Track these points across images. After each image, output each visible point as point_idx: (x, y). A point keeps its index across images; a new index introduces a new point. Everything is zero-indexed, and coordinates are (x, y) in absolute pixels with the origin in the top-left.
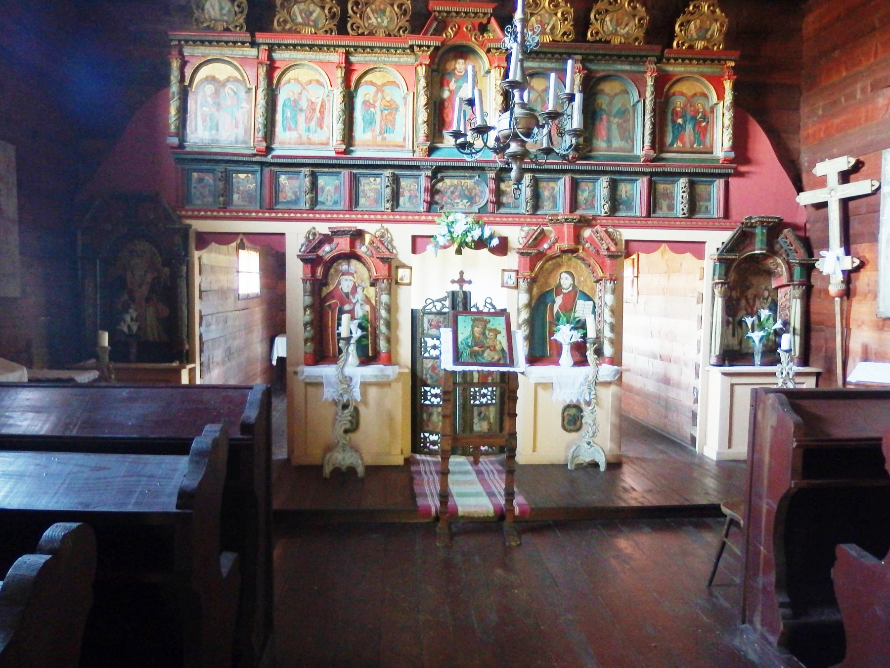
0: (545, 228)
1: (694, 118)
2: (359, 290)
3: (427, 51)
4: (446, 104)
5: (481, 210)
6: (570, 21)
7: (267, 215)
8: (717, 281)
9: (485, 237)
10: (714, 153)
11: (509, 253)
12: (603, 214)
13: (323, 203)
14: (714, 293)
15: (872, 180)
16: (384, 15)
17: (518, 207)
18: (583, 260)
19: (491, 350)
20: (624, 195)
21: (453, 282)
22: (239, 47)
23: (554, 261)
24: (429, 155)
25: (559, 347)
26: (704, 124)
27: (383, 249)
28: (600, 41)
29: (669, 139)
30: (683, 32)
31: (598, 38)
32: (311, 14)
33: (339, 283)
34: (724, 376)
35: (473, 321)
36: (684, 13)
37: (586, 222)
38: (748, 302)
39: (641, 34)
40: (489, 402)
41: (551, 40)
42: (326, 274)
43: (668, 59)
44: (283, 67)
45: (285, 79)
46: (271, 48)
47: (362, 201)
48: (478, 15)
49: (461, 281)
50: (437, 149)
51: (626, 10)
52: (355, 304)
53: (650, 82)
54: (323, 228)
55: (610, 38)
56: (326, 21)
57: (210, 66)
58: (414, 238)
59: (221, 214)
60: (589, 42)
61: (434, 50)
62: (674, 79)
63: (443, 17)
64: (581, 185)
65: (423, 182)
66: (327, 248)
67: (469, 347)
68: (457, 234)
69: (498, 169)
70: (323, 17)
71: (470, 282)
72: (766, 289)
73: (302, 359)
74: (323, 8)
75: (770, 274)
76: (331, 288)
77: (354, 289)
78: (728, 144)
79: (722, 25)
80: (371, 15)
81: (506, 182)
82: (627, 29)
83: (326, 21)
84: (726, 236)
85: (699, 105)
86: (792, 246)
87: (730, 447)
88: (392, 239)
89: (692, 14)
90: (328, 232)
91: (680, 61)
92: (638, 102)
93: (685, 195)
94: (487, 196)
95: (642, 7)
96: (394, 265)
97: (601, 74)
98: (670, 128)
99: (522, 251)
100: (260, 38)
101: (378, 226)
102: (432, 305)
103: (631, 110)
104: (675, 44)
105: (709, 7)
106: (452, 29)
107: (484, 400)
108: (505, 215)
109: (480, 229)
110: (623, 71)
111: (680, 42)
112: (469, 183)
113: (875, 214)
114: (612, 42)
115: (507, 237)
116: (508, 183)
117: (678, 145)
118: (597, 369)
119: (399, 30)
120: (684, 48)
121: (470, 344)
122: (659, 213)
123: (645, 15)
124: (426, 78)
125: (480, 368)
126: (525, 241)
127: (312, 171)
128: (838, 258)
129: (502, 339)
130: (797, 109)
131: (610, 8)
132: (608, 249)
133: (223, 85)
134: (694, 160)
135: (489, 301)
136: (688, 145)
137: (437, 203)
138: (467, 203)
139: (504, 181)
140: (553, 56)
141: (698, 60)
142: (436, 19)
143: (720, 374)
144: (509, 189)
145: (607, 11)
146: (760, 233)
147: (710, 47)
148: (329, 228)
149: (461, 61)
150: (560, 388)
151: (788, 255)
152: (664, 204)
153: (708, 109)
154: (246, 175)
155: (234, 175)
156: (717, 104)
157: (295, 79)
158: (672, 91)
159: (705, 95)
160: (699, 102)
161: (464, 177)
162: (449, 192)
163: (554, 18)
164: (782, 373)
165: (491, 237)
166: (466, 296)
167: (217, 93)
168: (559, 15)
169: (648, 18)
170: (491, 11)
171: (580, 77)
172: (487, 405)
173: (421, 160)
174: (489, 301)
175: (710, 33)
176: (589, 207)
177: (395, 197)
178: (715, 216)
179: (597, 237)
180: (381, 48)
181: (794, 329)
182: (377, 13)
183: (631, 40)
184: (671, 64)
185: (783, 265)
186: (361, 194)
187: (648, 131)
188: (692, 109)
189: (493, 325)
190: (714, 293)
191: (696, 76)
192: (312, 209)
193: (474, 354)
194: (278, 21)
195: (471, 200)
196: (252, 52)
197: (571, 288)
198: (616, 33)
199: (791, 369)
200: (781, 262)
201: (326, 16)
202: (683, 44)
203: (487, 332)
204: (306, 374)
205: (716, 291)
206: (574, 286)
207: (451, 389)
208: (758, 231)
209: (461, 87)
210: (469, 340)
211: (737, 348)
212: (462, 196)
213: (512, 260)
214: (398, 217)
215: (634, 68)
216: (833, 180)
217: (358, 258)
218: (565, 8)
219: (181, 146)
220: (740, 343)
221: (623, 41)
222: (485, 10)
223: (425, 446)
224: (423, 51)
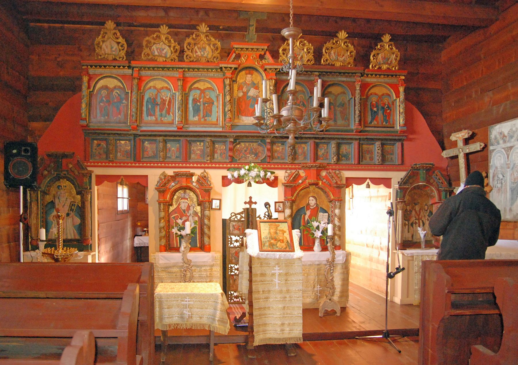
2: (191, 208)
3: (230, 70)
21: (245, 203)
26: (388, 111)
30: (375, 60)
32: (163, 50)
43: (367, 75)
49: (250, 202)
54: (170, 172)
60: (322, 65)
70: (170, 51)
71: (256, 203)
72: (426, 205)
74: (170, 46)
75: (430, 196)
77: (189, 207)
78: (402, 122)
79: (396, 56)
80: (198, 50)
82: (343, 58)
84: (403, 174)
90: (172, 174)
92: (352, 98)
104: (371, 66)
105: (389, 46)
106: (244, 57)
114: (335, 65)
120: (376, 68)
122: (364, 162)
136: (380, 123)
138: (254, 156)
141: (384, 75)
148: (174, 172)
152: (368, 156)
158: (370, 93)
159: (389, 95)
163: (302, 52)
168: (305, 50)
175: (390, 60)
178: (397, 163)
179: (330, 176)
193: (271, 245)
194: (144, 54)
197: (315, 206)
198: (337, 60)
202: (375, 66)
206: (317, 204)
211: (410, 239)
215: (349, 79)
221: (342, 64)
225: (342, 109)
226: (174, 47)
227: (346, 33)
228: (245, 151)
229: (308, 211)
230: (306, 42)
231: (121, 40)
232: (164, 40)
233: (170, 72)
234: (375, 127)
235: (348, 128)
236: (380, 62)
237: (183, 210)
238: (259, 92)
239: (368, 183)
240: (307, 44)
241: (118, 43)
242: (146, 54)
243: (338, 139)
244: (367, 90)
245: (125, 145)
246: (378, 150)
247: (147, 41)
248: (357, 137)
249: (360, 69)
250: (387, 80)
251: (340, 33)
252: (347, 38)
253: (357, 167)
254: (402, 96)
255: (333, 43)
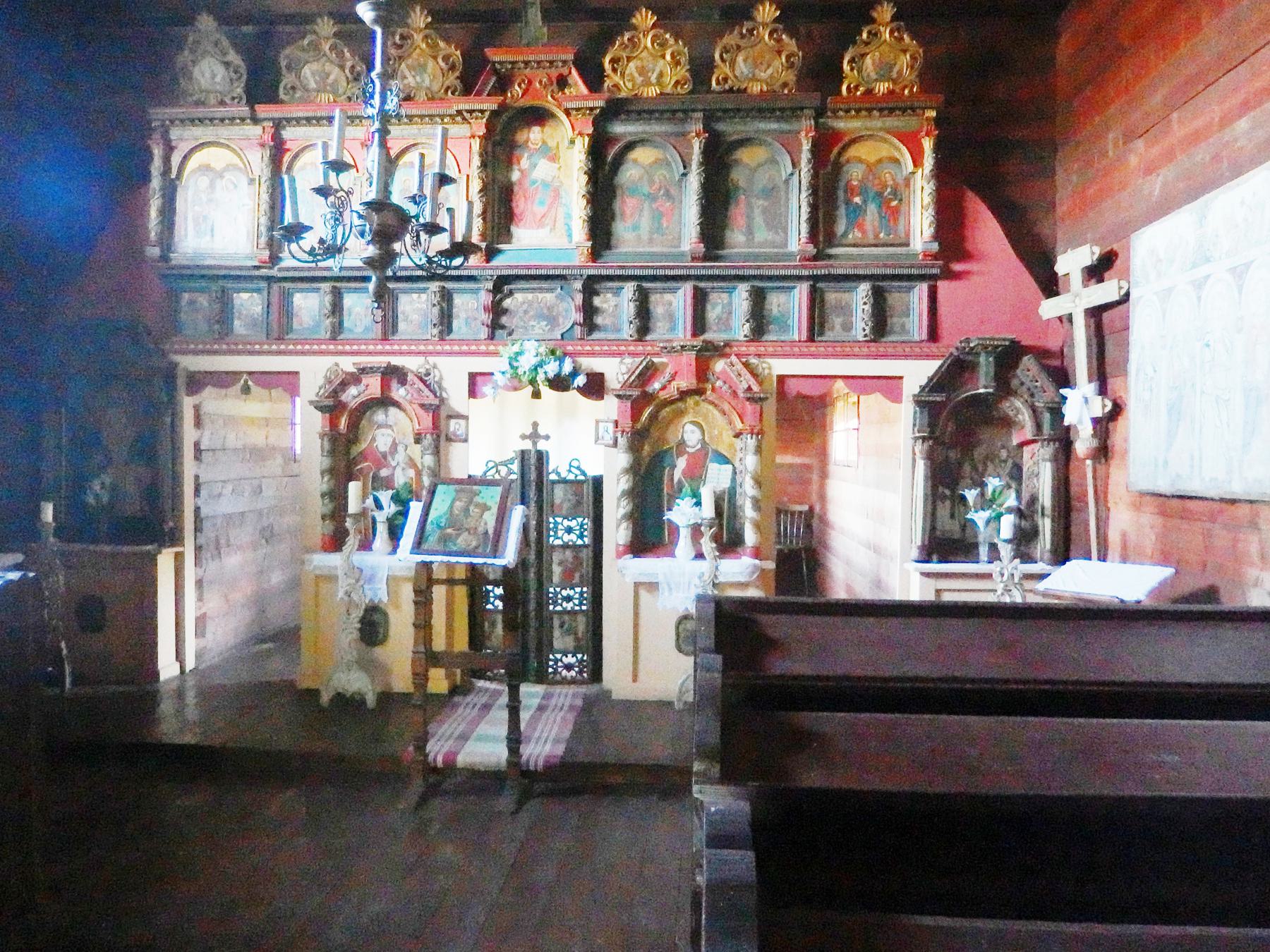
0: (656, 360)
1: (880, 194)
2: (400, 448)
3: (482, 118)
4: (516, 189)
5: (565, 335)
6: (685, 65)
7: (274, 347)
8: (917, 435)
9: (563, 373)
10: (912, 245)
11: (605, 396)
12: (861, 339)
13: (350, 330)
14: (914, 454)
15: (1119, 280)
16: (425, 71)
17: (619, 330)
18: (712, 403)
19: (469, 533)
20: (775, 311)
21: (524, 437)
22: (237, 124)
23: (673, 406)
24: (488, 261)
25: (674, 530)
26: (894, 203)
27: (427, 392)
28: (731, 90)
29: (841, 227)
30: (855, 72)
31: (727, 87)
32: (328, 75)
33: (374, 439)
34: (926, 579)
35: (457, 491)
36: (855, 43)
37: (719, 350)
38: (975, 468)
39: (790, 77)
40: (577, 608)
41: (659, 92)
42: (354, 425)
43: (835, 112)
44: (295, 150)
45: (298, 164)
46: (278, 125)
47: (402, 326)
48: (555, 64)
49: (534, 436)
50: (499, 251)
51: (767, 44)
52: (395, 468)
53: (806, 146)
54: (348, 364)
55: (745, 85)
56: (348, 84)
57: (212, 149)
58: (473, 377)
59: (216, 347)
60: (713, 92)
61: (490, 117)
62: (846, 139)
63: (507, 69)
64: (711, 297)
65: (485, 298)
66: (353, 391)
67: (439, 527)
68: (523, 370)
69: (585, 277)
70: (344, 79)
71: (547, 437)
72: (1003, 447)
73: (320, 543)
74: (342, 67)
75: (1008, 423)
76: (363, 446)
77: (394, 446)
78: (929, 231)
79: (913, 58)
80: (407, 73)
81: (602, 295)
82: (770, 71)
83: (348, 84)
84: (930, 367)
85: (887, 175)
86: (1037, 381)
87: (635, 680)
88: (441, 378)
89: (867, 44)
90: (352, 369)
91: (853, 113)
92: (792, 174)
93: (867, 307)
94: (571, 314)
95: (791, 39)
96: (443, 413)
97: (735, 137)
98: (842, 211)
99: (621, 393)
100: (263, 110)
101: (421, 359)
102: (494, 470)
103: (782, 186)
104: (844, 88)
105: (891, 32)
106: (519, 85)
107: (569, 606)
108: (615, 342)
109: (558, 363)
110: (768, 132)
111: (852, 86)
112: (549, 297)
113: (1125, 332)
114: (749, 91)
115: (602, 374)
116: (605, 296)
117: (855, 235)
118: (715, 564)
119: (446, 91)
120: (858, 93)
121: (443, 525)
122: (829, 335)
123: (796, 49)
124: (481, 155)
125: (446, 559)
126: (626, 377)
127: (334, 287)
128: (1086, 400)
129: (490, 519)
130: (1053, 172)
131: (742, 43)
132: (749, 389)
133: (221, 175)
134: (877, 257)
135: (575, 464)
136: (871, 236)
137: (503, 327)
138: (546, 326)
139: (598, 294)
140: (674, 115)
141: (881, 110)
142: (496, 72)
143: (918, 574)
144: (605, 306)
145: (739, 47)
146: (986, 365)
147: (897, 90)
148: (354, 364)
149: (536, 129)
150: (670, 589)
151: (1032, 395)
152: (837, 321)
153: (900, 180)
154: (250, 294)
155: (235, 295)
156: (913, 173)
157: (312, 163)
158: (843, 159)
159: (896, 161)
160: (886, 171)
161: (541, 290)
162: (521, 310)
163: (662, 62)
164: (1002, 575)
165: (575, 373)
166: (541, 457)
167: (212, 186)
168: (668, 57)
169: (800, 54)
170: (571, 57)
171: (700, 142)
172: (572, 613)
173: (477, 268)
174: (575, 464)
175: (896, 70)
176: (723, 328)
177: (446, 320)
178: (917, 338)
179: (733, 371)
180: (422, 117)
181: (1043, 508)
182: (414, 69)
183: (777, 87)
184: (841, 118)
185: (1024, 411)
186: (400, 316)
187: (805, 216)
188: (876, 182)
189: (483, 498)
190: (914, 454)
191: (881, 134)
192: (333, 338)
193: (445, 539)
194: (285, 88)
195: (552, 320)
196: (256, 130)
197: (699, 446)
198: (754, 79)
199: (1016, 569)
200: (1021, 406)
201: (347, 78)
202: (857, 88)
203: (471, 508)
204: (315, 563)
205: (917, 450)
207: (423, 587)
208: (982, 359)
209: (536, 164)
210: (443, 520)
211: (957, 536)
212: (541, 317)
213: (610, 408)
214: (447, 348)
215: (785, 126)
216: (1076, 279)
217: (396, 404)
218: (675, 48)
219: (165, 258)
220: (963, 528)
221: (765, 88)
222: (564, 57)
223: (555, 672)
224: (476, 118)
225: (766, 204)
226: (353, 67)
227: (774, 7)
228: (526, 312)
229: (680, 459)
230: (668, 36)
231: (233, 57)
232: (328, 52)
233: (415, 126)
234: (854, 245)
235: (786, 250)
236: (868, 76)
237: (381, 453)
238: (559, 169)
239: (246, 381)
240: (672, 41)
241: (227, 64)
242: (289, 86)
243: (755, 277)
244: (836, 151)
245: (249, 303)
246: (865, 303)
247: (287, 57)
248: (805, 272)
249: (814, 99)
250: (892, 122)
251: (761, 8)
252: (776, 20)
253: (380, 347)
254: (929, 161)
255: (741, 34)
